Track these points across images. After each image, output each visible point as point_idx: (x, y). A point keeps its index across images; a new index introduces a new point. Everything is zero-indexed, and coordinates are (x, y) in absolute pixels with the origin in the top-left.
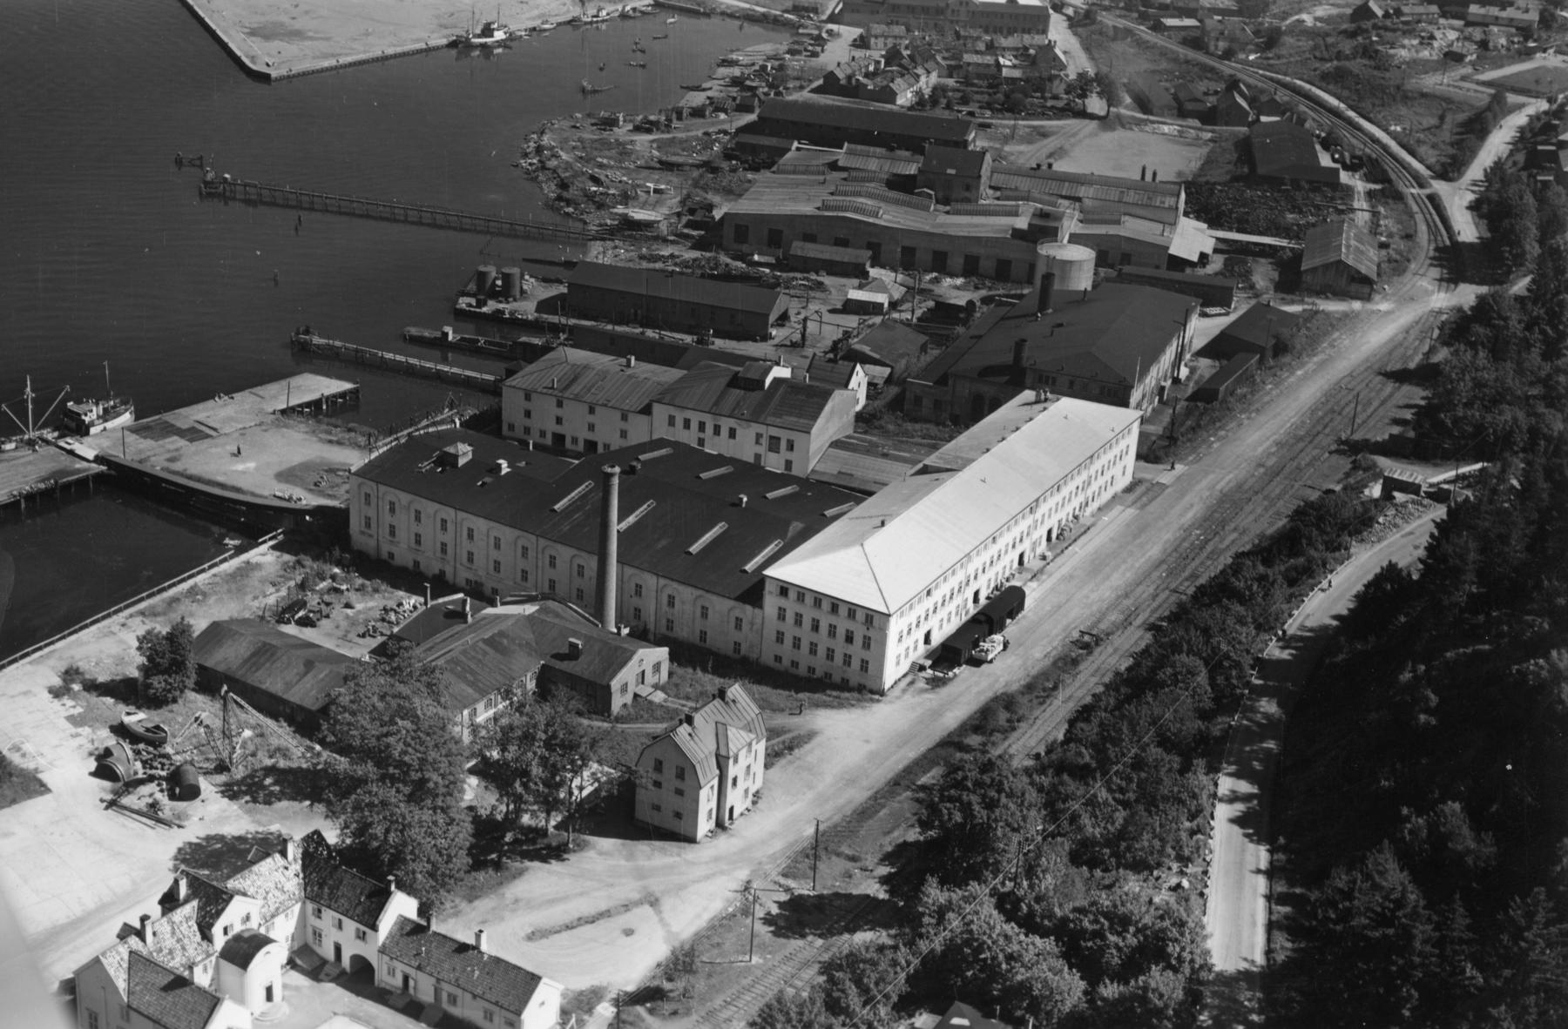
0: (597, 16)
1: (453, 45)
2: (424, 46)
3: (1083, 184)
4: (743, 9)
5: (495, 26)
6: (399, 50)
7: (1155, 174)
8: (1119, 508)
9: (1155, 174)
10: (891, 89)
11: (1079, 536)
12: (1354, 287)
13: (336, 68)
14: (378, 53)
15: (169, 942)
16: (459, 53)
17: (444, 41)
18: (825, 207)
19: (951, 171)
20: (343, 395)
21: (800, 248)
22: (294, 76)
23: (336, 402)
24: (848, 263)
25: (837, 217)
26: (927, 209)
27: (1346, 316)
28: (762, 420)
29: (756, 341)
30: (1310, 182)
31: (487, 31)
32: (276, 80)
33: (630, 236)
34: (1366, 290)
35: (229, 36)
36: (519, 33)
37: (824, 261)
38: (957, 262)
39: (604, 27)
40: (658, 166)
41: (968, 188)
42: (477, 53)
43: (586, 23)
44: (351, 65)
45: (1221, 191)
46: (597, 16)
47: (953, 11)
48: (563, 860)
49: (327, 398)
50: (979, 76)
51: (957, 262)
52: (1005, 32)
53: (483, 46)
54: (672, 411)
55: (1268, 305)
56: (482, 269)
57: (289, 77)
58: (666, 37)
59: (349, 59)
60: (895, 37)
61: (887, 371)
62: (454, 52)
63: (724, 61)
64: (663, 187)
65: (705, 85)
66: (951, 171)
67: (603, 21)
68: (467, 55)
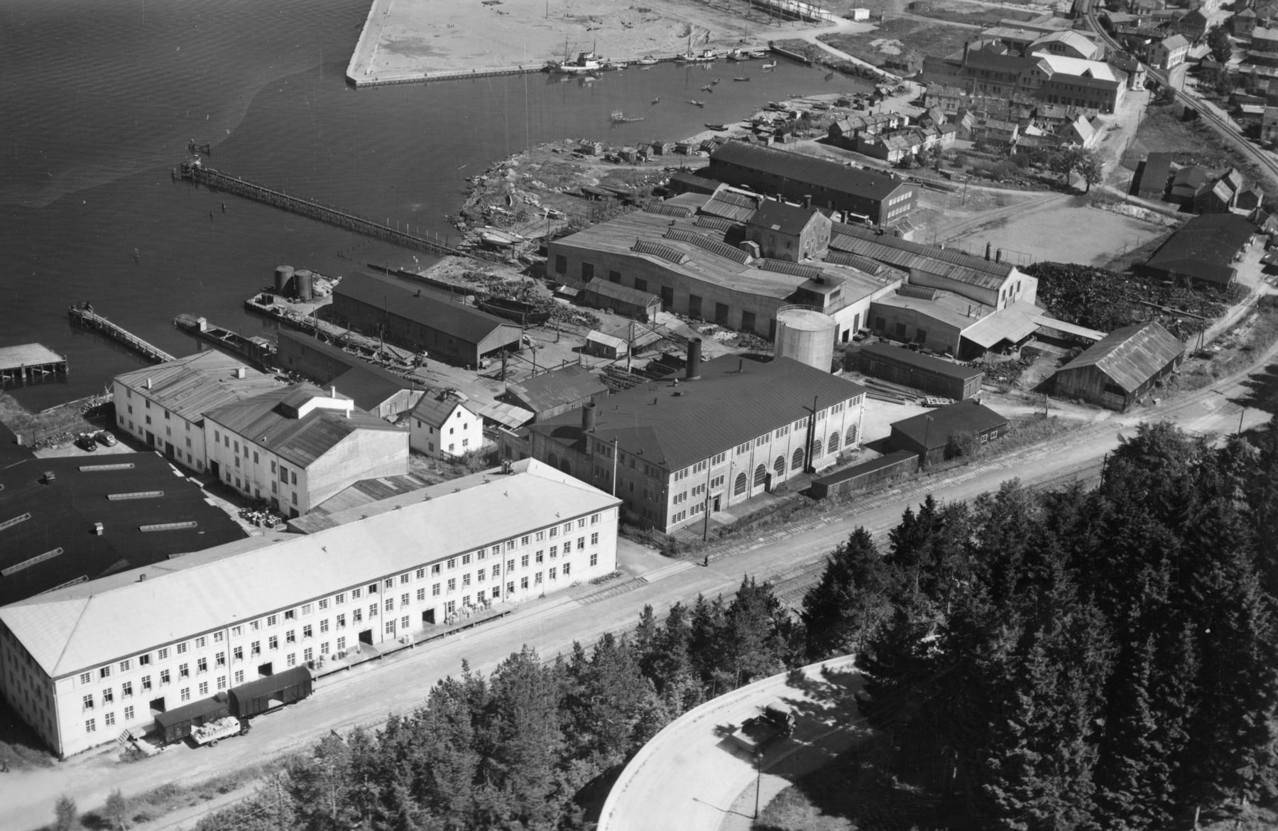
0: (703, 57)
1: (545, 70)
2: (517, 69)
3: (918, 254)
4: (843, 61)
5: (590, 56)
6: (490, 70)
7: (998, 253)
8: (567, 598)
9: (998, 253)
10: (884, 146)
11: (483, 622)
12: (1108, 396)
13: (423, 81)
14: (469, 71)
15: (552, 699)
16: (550, 78)
17: (540, 66)
18: (638, 247)
19: (776, 227)
20: (48, 367)
21: (600, 285)
22: (379, 84)
23: (40, 373)
24: (632, 305)
25: (638, 259)
26: (741, 261)
27: (1078, 425)
28: (274, 449)
29: (466, 369)
30: (1194, 280)
31: (581, 62)
32: (361, 86)
33: (482, 255)
34: (1120, 401)
35: (365, 43)
36: (615, 65)
37: (613, 299)
38: (736, 317)
39: (709, 66)
40: (582, 194)
41: (789, 245)
42: (565, 79)
43: (689, 62)
44: (439, 79)
45: (1099, 278)
46: (703, 57)
47: (1025, 79)
48: (763, 709)
49: (28, 370)
50: (990, 141)
51: (736, 317)
52: (1060, 101)
53: (572, 74)
54: (218, 428)
55: (977, 403)
56: (280, 269)
57: (374, 85)
58: (747, 80)
59: (437, 74)
60: (949, 98)
61: (530, 415)
62: (547, 76)
63: (772, 106)
64: (557, 213)
65: (725, 127)
66: (776, 227)
67: (707, 61)
68: (557, 80)
